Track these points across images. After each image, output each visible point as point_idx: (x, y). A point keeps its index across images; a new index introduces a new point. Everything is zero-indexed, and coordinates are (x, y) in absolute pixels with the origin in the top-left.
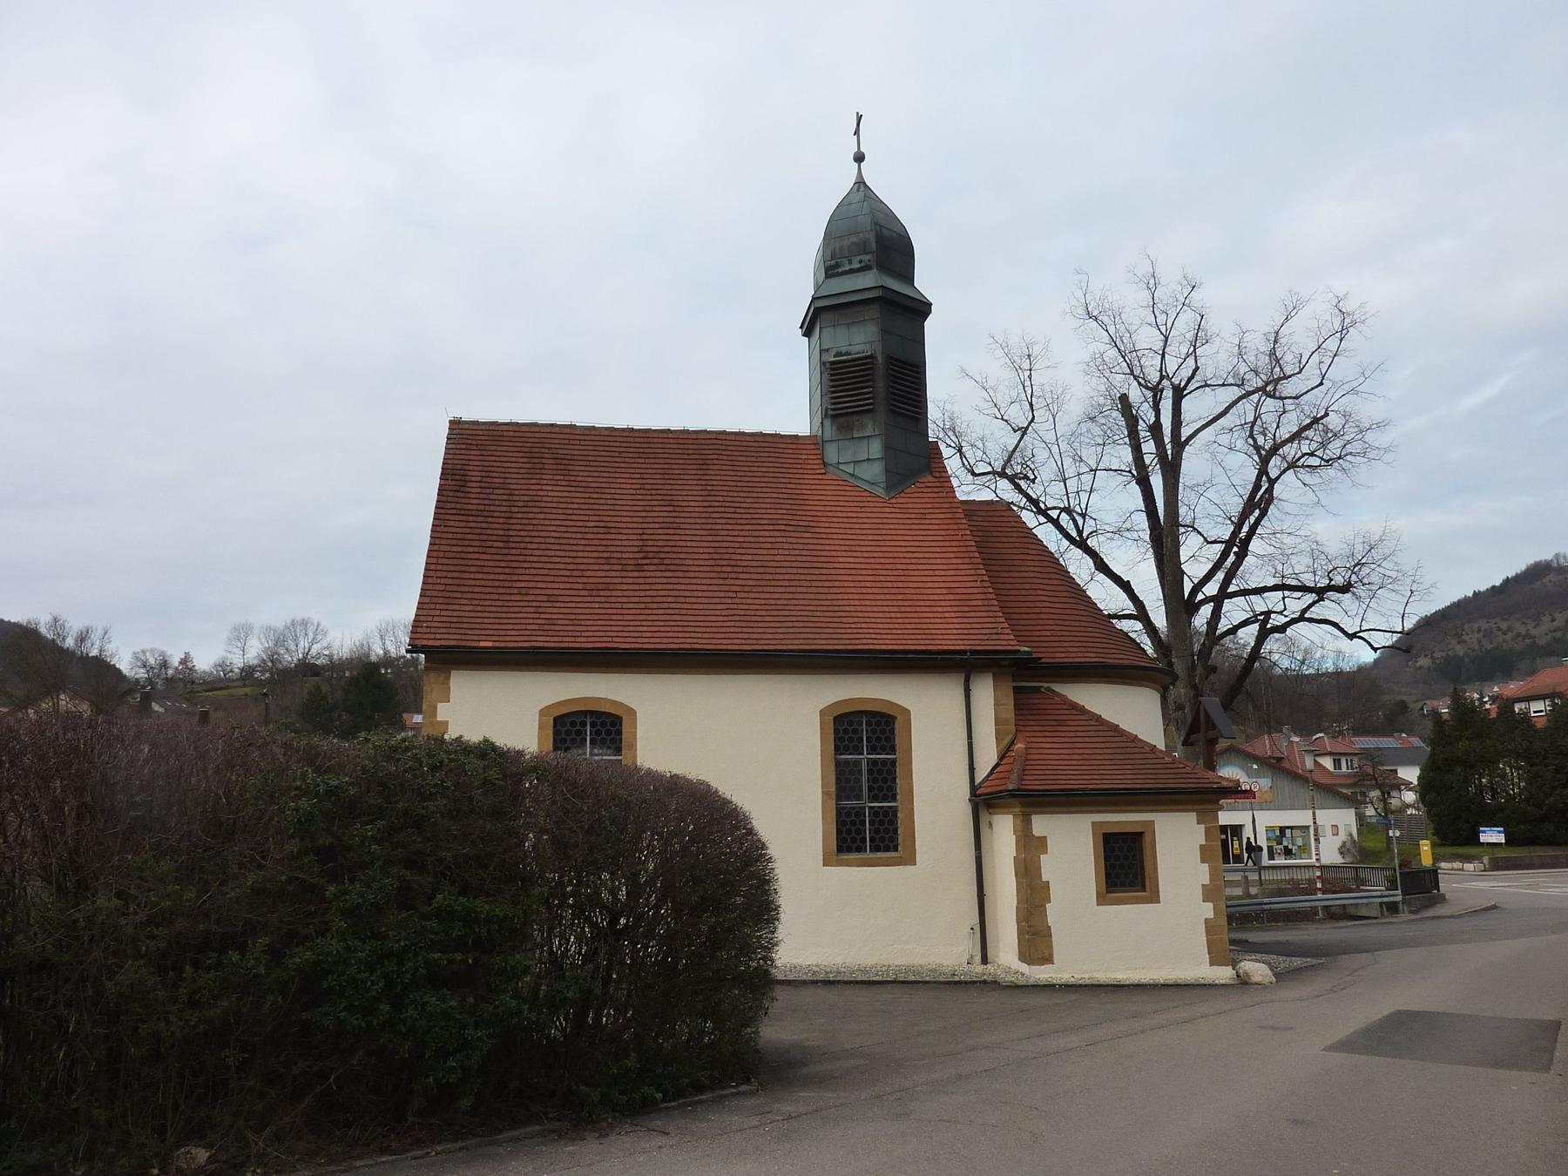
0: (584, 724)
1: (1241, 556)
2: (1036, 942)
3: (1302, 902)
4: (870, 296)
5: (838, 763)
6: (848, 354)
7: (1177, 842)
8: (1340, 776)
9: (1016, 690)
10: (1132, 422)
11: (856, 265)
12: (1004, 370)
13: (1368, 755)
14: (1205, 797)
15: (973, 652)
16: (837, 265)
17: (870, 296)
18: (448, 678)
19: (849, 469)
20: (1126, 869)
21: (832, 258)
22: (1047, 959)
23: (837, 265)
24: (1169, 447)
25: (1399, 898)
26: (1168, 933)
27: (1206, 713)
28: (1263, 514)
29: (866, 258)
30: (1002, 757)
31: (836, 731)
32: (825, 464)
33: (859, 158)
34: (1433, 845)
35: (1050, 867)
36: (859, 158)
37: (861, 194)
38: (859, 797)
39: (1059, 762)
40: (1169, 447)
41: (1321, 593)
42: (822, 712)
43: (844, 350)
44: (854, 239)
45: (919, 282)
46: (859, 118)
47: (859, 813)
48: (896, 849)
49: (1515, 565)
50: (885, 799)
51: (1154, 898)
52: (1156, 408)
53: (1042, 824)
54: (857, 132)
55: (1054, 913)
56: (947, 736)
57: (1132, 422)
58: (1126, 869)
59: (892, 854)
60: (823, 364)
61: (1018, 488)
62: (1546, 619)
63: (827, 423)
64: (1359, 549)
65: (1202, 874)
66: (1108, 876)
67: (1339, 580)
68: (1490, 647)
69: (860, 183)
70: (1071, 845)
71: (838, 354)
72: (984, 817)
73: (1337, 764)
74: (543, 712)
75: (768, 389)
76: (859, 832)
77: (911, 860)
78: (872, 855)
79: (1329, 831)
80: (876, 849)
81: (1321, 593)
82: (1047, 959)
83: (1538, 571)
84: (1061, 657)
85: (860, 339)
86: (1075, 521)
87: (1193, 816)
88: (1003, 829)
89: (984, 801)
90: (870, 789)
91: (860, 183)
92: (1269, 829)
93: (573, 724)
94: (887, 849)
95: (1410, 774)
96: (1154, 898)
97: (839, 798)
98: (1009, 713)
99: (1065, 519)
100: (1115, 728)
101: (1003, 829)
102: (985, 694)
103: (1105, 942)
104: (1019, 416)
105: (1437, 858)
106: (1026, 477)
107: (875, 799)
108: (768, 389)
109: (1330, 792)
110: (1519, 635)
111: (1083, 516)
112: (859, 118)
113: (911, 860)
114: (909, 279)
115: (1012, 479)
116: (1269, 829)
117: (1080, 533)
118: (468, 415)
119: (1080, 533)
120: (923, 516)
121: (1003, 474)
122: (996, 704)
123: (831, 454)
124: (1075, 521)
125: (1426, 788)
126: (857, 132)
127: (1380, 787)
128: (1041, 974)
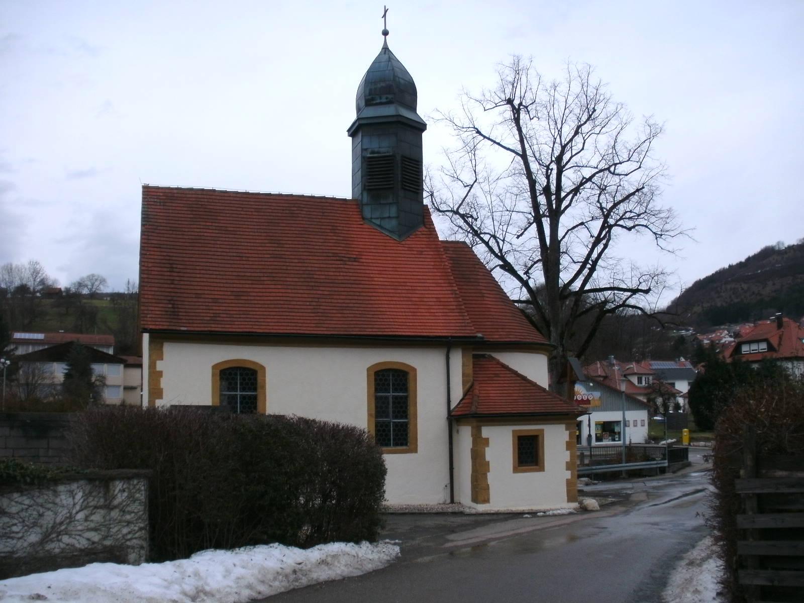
0: (236, 374)
1: (593, 270)
2: (480, 491)
3: (615, 467)
4: (388, 115)
5: (377, 398)
6: (378, 153)
7: (555, 441)
8: (640, 388)
9: (475, 356)
10: (532, 183)
11: (384, 100)
12: (467, 172)
13: (660, 375)
14: (569, 415)
15: (452, 337)
16: (373, 99)
17: (388, 115)
18: (162, 347)
19: (378, 222)
20: (528, 454)
21: (370, 94)
22: (487, 501)
23: (373, 99)
24: (554, 202)
25: (666, 465)
26: (546, 490)
27: (570, 363)
28: (606, 246)
29: (390, 96)
30: (465, 395)
31: (376, 380)
32: (363, 218)
33: (385, 33)
34: (691, 431)
35: (490, 454)
36: (385, 33)
37: (387, 56)
38: (387, 416)
39: (495, 396)
40: (554, 202)
41: (634, 291)
42: (369, 370)
43: (376, 150)
44: (383, 84)
45: (420, 111)
46: (386, 11)
47: (387, 425)
48: (406, 445)
49: (754, 249)
50: (402, 418)
51: (542, 469)
52: (548, 177)
53: (487, 432)
54: (385, 16)
55: (491, 478)
56: (436, 382)
57: (532, 183)
58: (528, 454)
59: (404, 447)
60: (363, 158)
61: (466, 221)
62: (770, 283)
63: (365, 194)
64: (660, 270)
65: (566, 456)
66: (519, 458)
67: (643, 287)
68: (736, 301)
69: (386, 49)
70: (501, 443)
71: (373, 152)
72: (455, 428)
73: (640, 381)
74: (214, 367)
75: (327, 169)
76: (386, 435)
77: (415, 450)
78: (394, 448)
79: (631, 424)
80: (396, 444)
81: (634, 291)
82: (487, 501)
83: (767, 253)
84: (496, 337)
85: (383, 145)
86: (498, 243)
87: (563, 427)
88: (465, 435)
89: (455, 419)
90: (393, 412)
91: (386, 49)
92: (597, 424)
93: (230, 374)
94: (402, 445)
95: (683, 387)
96: (542, 469)
97: (377, 417)
98: (470, 371)
99: (492, 243)
100: (524, 378)
101: (465, 435)
102: (457, 360)
103: (512, 490)
104: (468, 178)
105: (692, 439)
106: (472, 217)
107: (396, 417)
108: (327, 169)
109: (632, 402)
110: (753, 293)
111: (503, 240)
112: (386, 11)
113: (415, 450)
114: (413, 108)
115: (463, 216)
116: (597, 424)
117: (501, 250)
118: (153, 183)
119: (501, 250)
120: (420, 253)
121: (456, 212)
122: (463, 365)
123: (367, 212)
124: (498, 243)
125: (691, 395)
126: (385, 16)
127: (662, 395)
128: (481, 508)
